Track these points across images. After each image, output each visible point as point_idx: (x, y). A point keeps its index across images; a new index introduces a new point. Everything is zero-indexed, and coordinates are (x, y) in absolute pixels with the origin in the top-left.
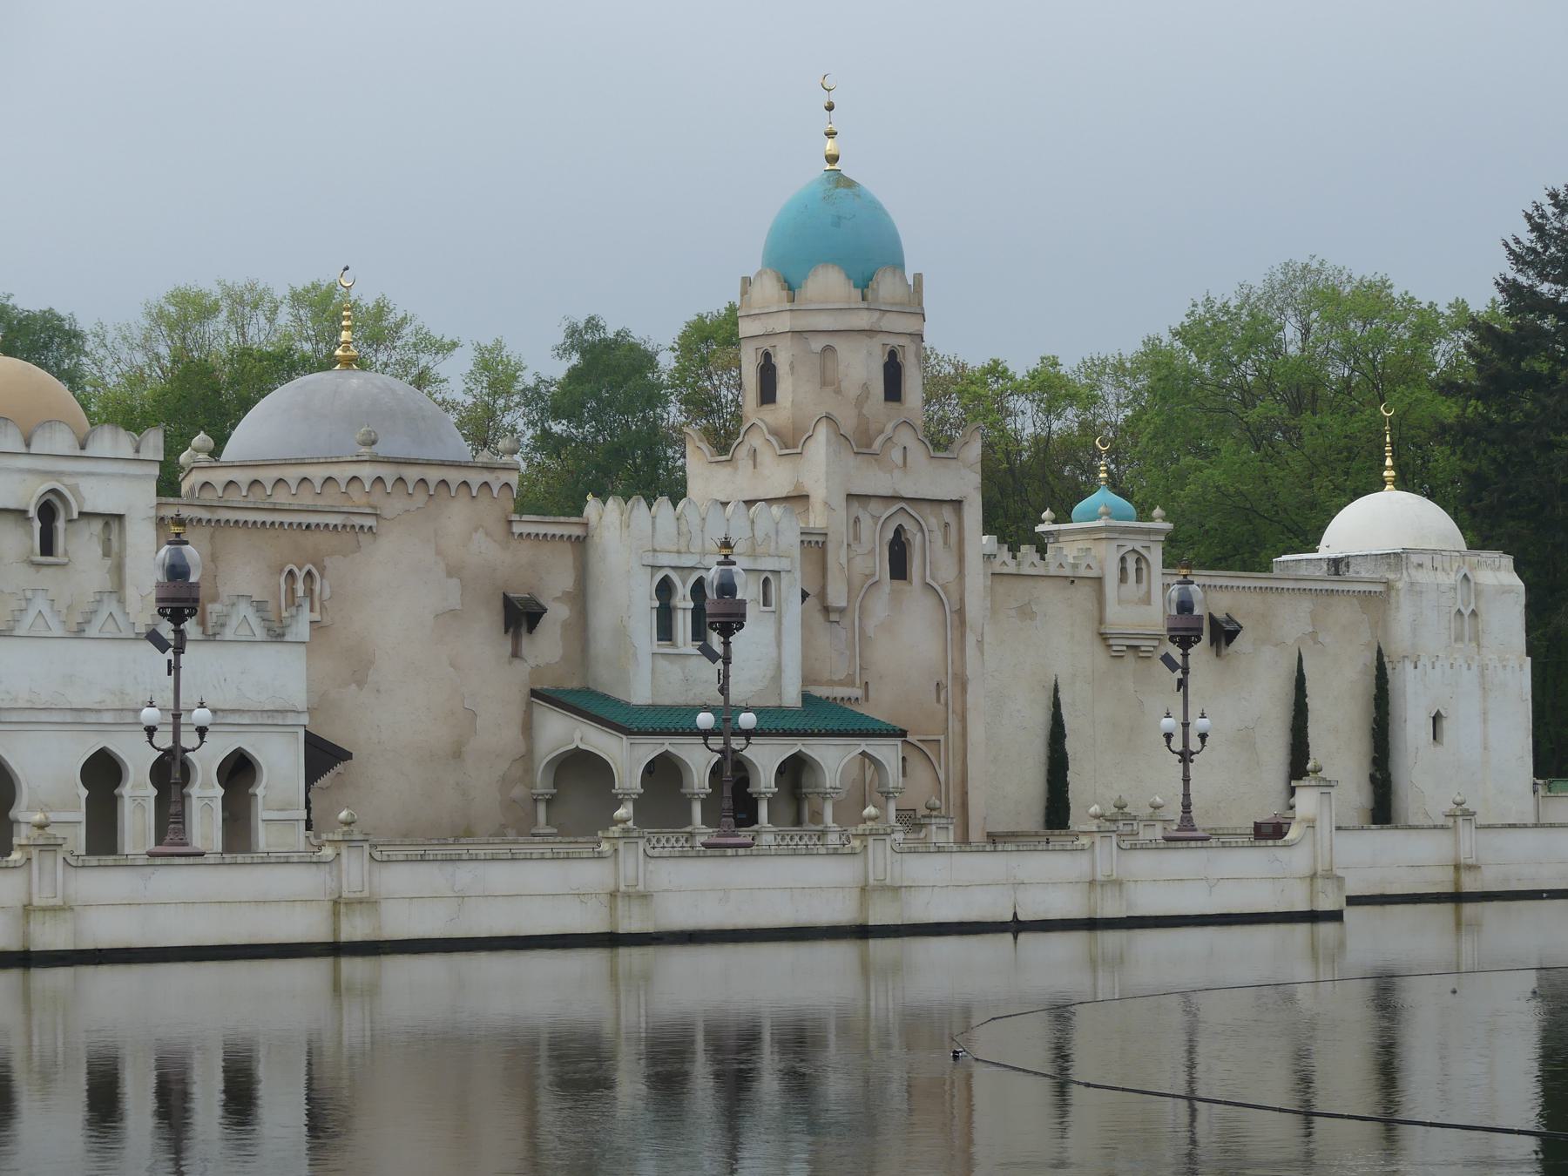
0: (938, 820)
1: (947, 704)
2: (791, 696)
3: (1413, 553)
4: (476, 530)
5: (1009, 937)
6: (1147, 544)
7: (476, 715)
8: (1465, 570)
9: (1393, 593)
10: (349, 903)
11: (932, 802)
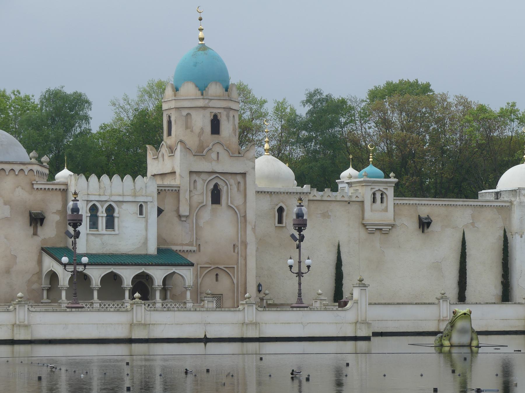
0: (208, 299)
1: (238, 253)
2: (152, 249)
3: (522, 190)
4: (18, 187)
5: (202, 344)
6: (386, 187)
7: (16, 257)
9: (513, 206)
11: (207, 291)
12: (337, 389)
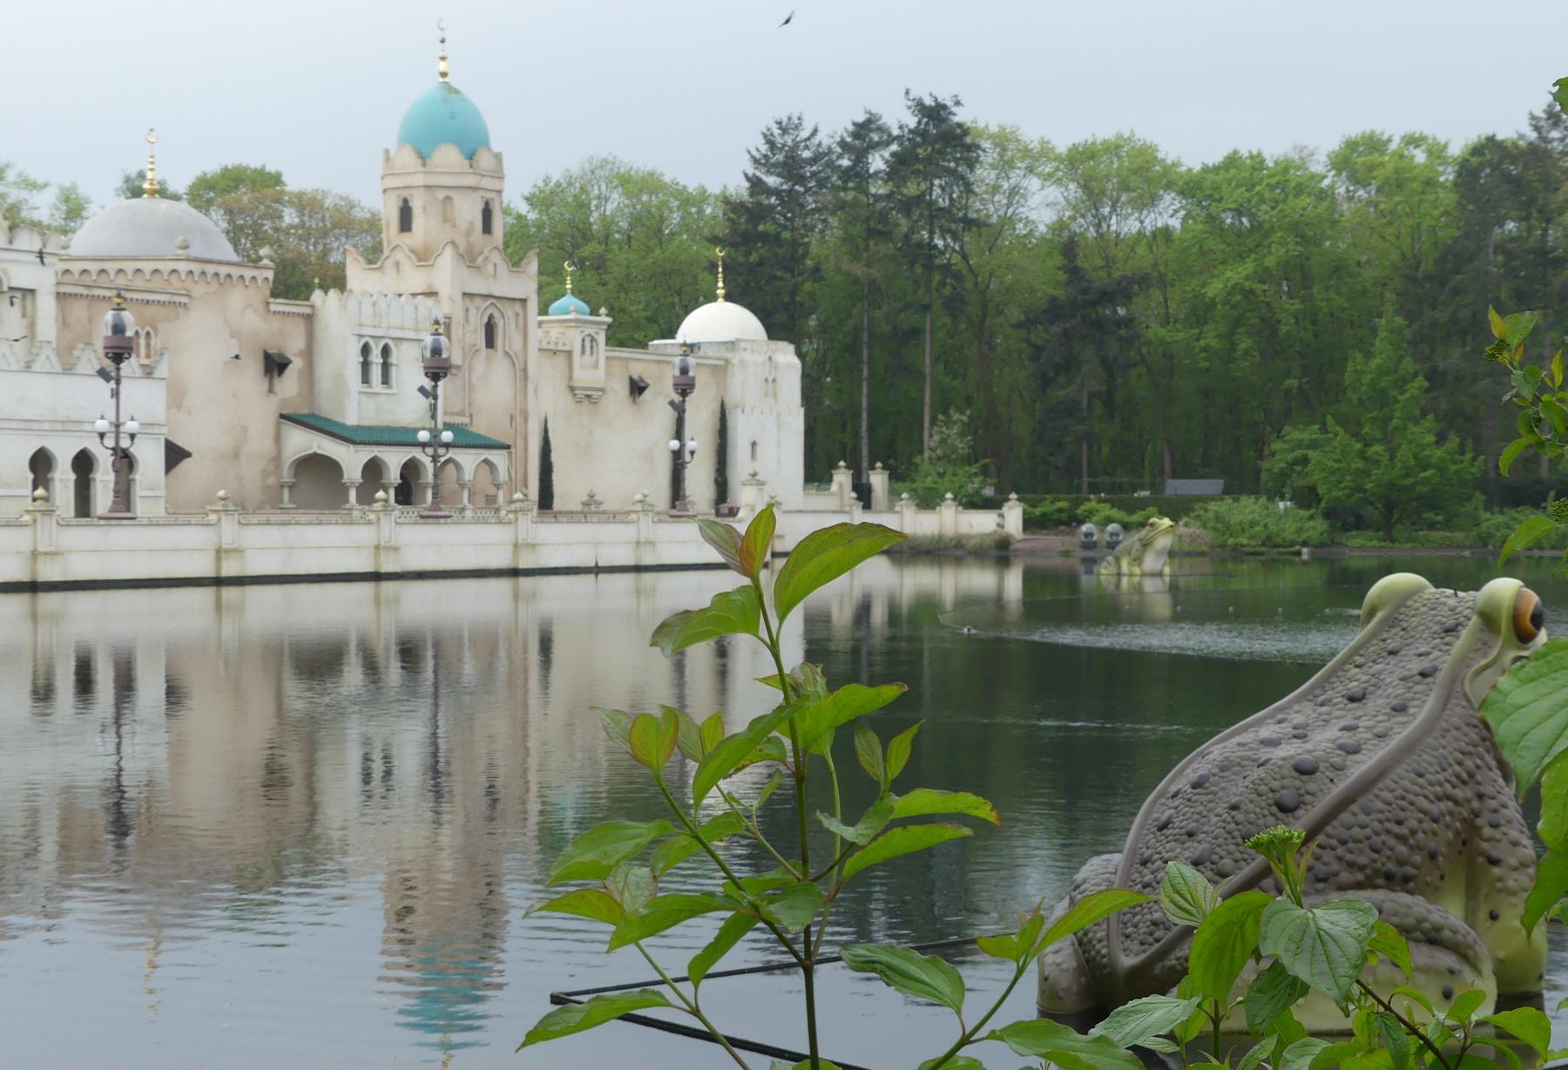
5: (592, 576)
8: (770, 353)
10: (227, 551)
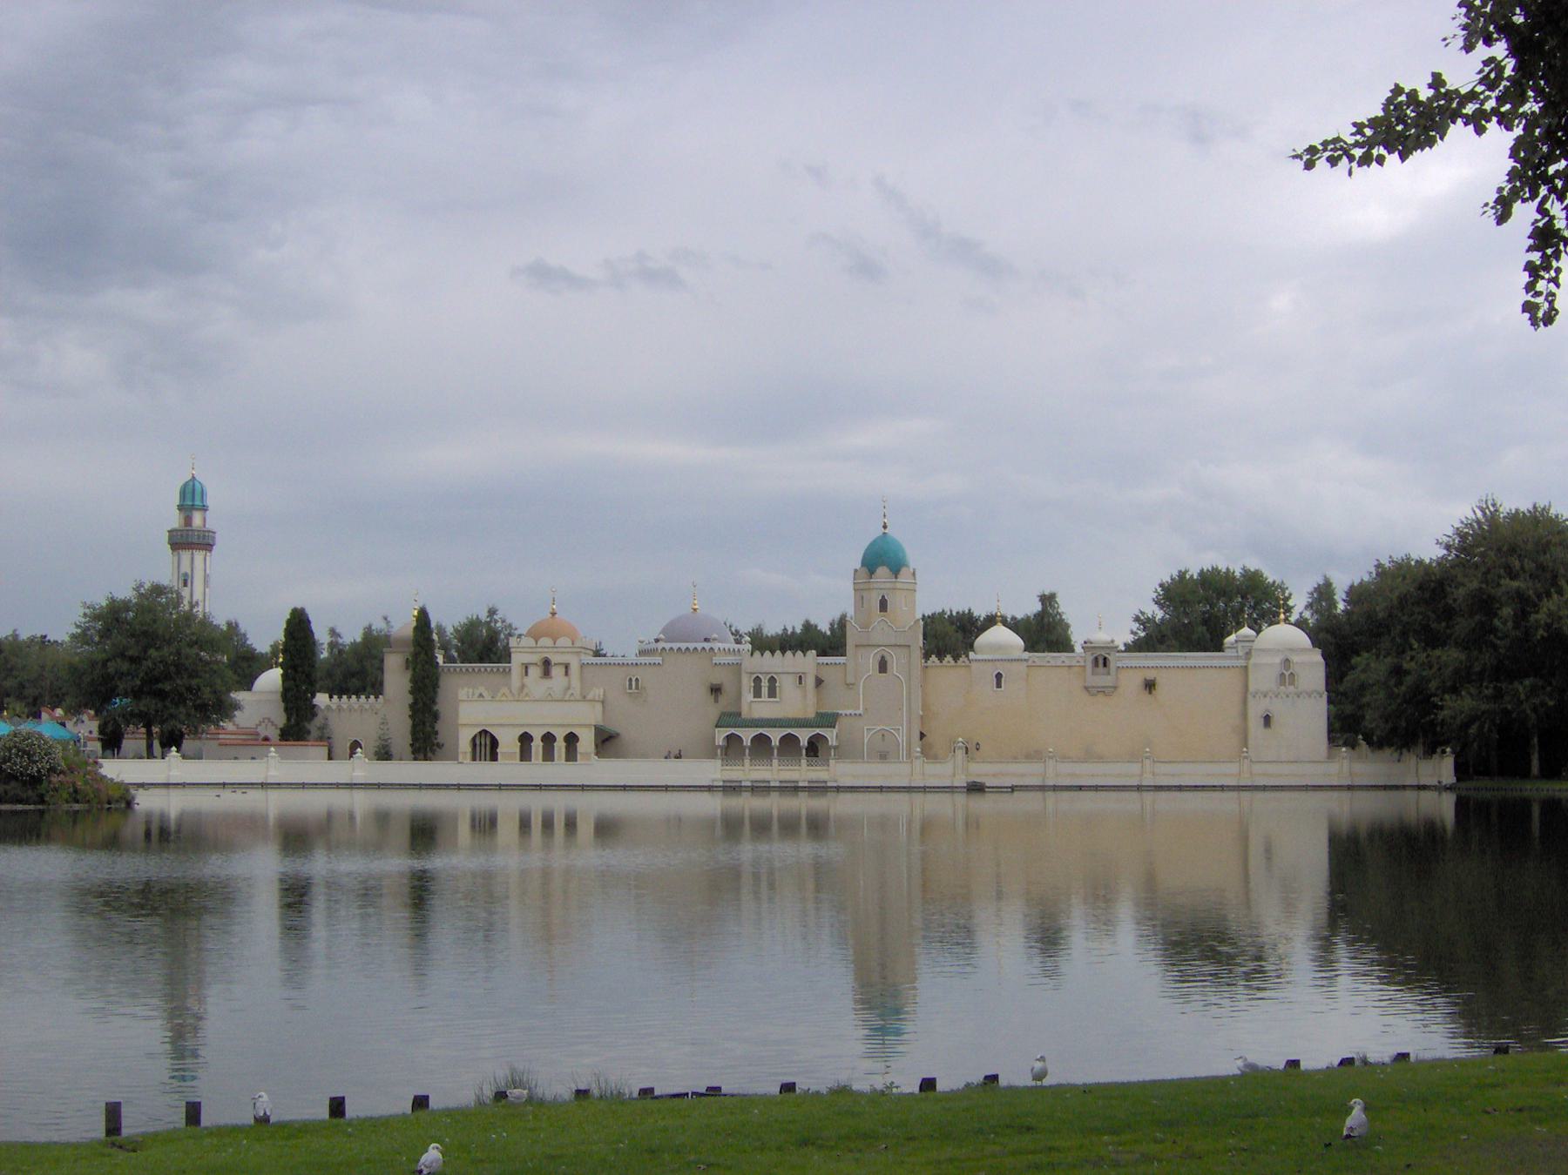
12: (1472, 802)
